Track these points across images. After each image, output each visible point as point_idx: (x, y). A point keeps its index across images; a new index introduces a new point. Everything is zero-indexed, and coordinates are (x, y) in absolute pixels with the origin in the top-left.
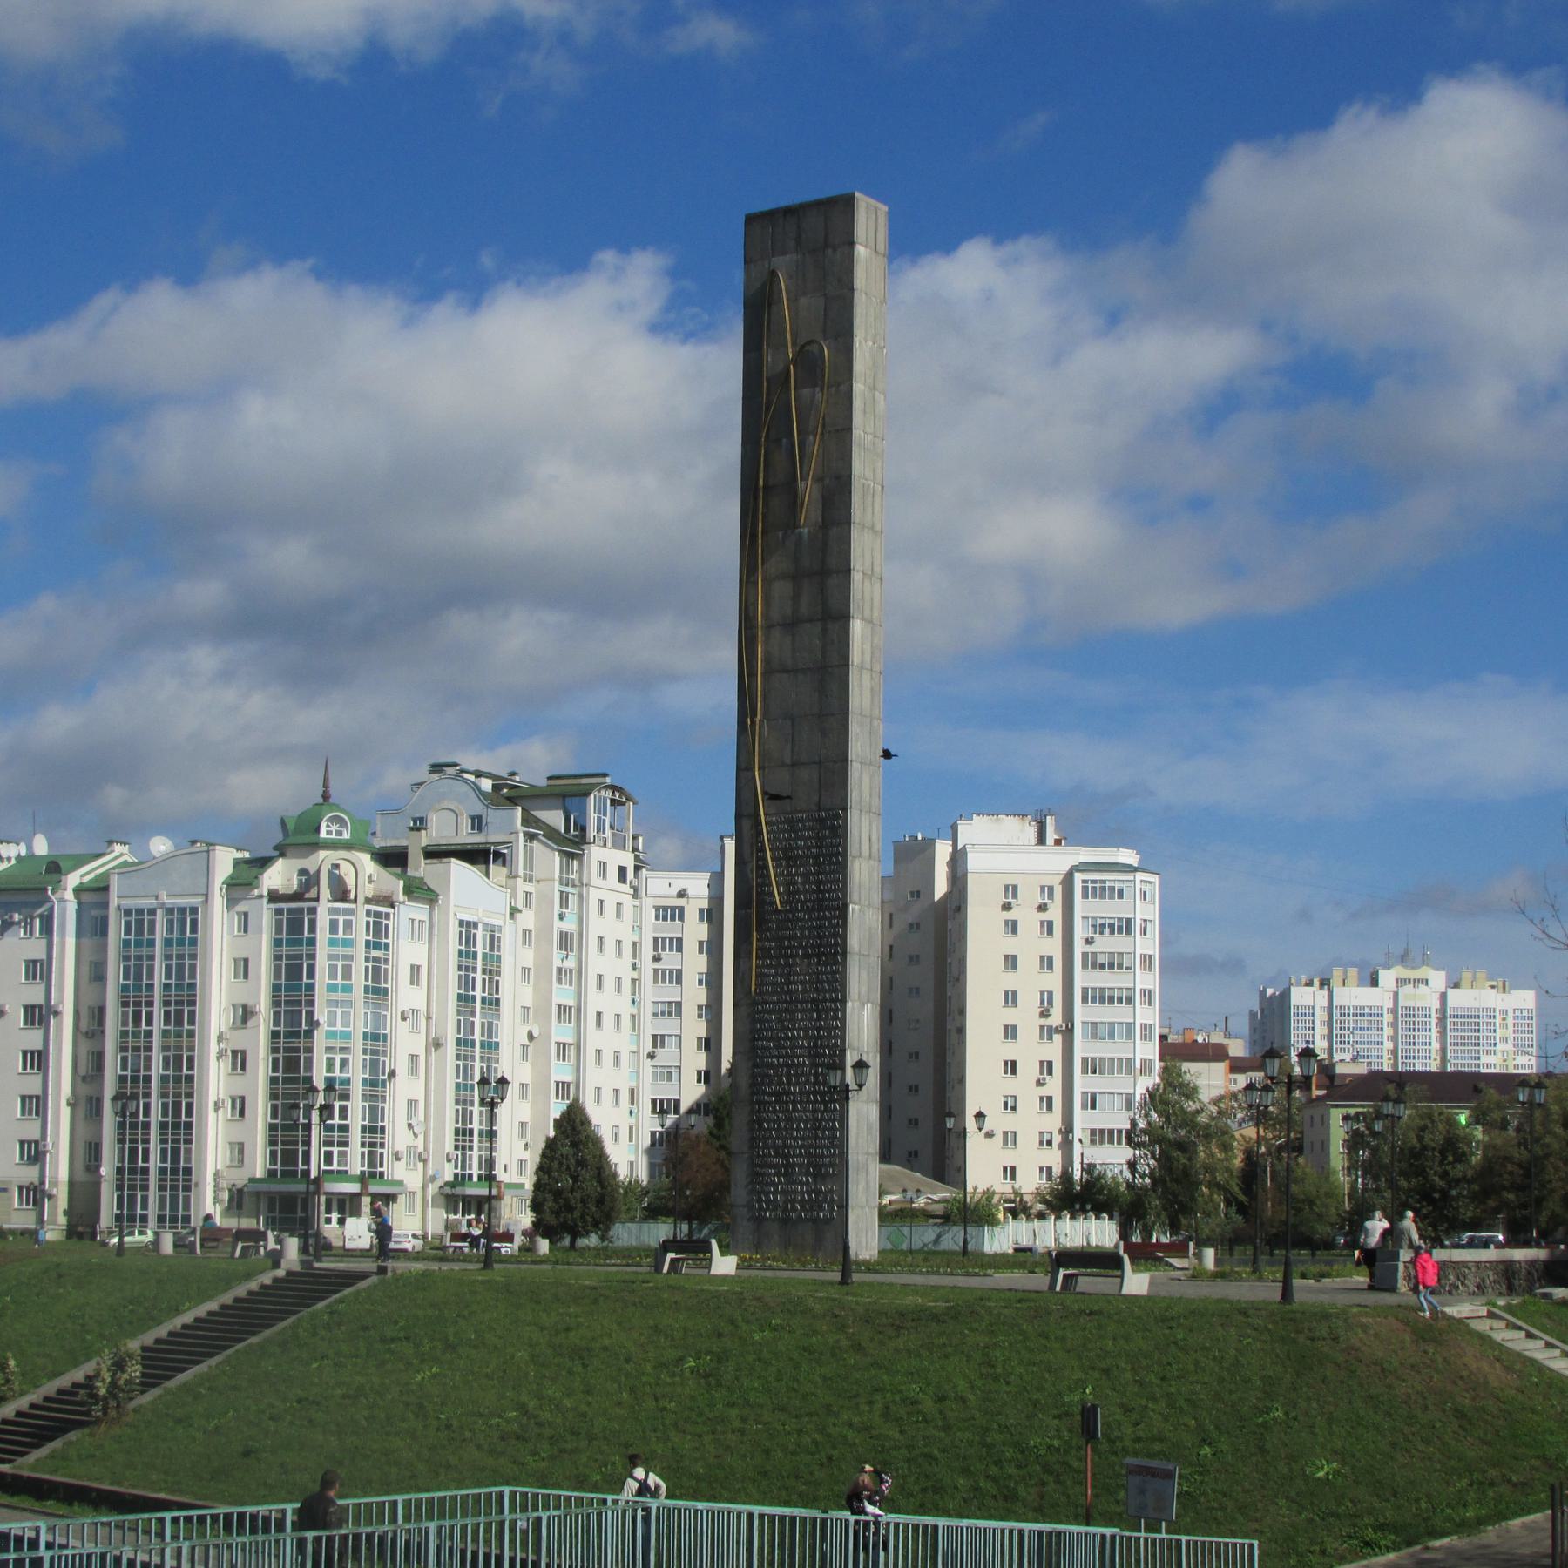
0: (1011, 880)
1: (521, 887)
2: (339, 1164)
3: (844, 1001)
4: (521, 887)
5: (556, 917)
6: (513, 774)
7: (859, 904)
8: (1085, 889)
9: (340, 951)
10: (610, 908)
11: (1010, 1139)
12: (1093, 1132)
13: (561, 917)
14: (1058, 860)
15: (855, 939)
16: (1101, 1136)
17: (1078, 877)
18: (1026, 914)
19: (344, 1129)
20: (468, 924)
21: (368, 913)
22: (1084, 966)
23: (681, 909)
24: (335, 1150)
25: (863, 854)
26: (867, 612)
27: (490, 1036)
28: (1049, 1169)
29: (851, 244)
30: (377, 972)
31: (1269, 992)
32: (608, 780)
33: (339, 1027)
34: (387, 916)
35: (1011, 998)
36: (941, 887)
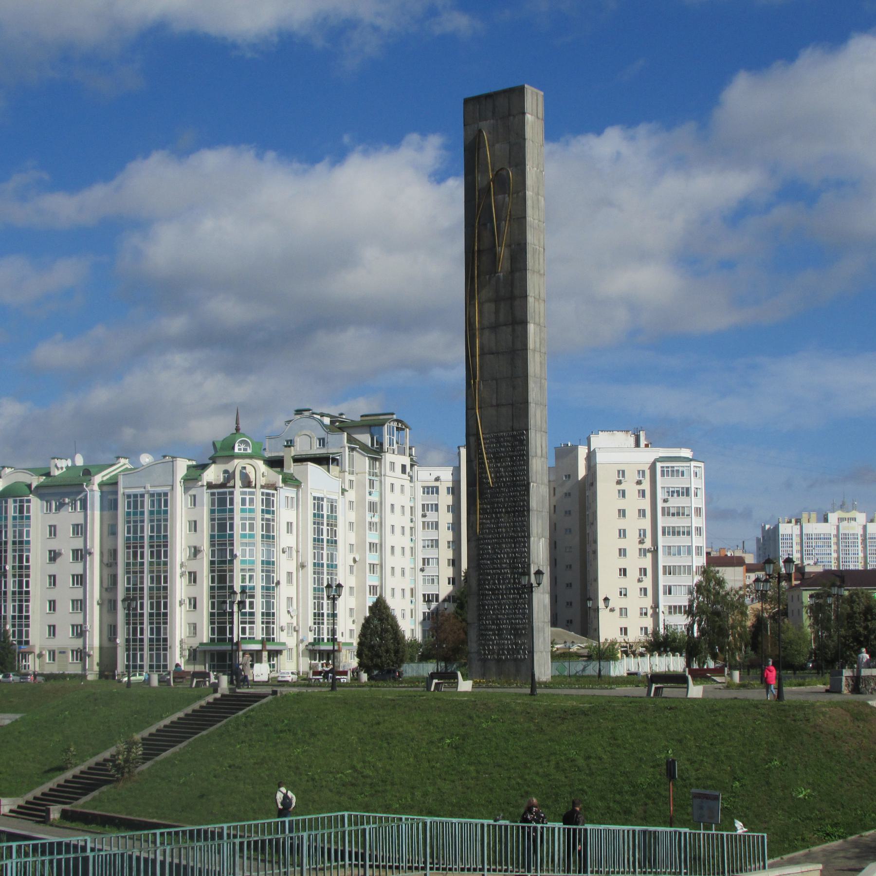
0: (621, 468)
3: (529, 537)
5: (367, 494)
6: (342, 414)
8: (663, 472)
10: (397, 488)
11: (624, 612)
12: (670, 607)
13: (370, 494)
14: (647, 456)
15: (534, 503)
16: (674, 609)
20: (318, 498)
21: (263, 494)
22: (663, 514)
23: (437, 488)
24: (247, 626)
26: (537, 320)
27: (332, 561)
28: (646, 628)
29: (524, 114)
30: (268, 527)
31: (767, 527)
32: (395, 417)
33: (248, 558)
34: (273, 495)
35: (622, 533)
36: (582, 473)
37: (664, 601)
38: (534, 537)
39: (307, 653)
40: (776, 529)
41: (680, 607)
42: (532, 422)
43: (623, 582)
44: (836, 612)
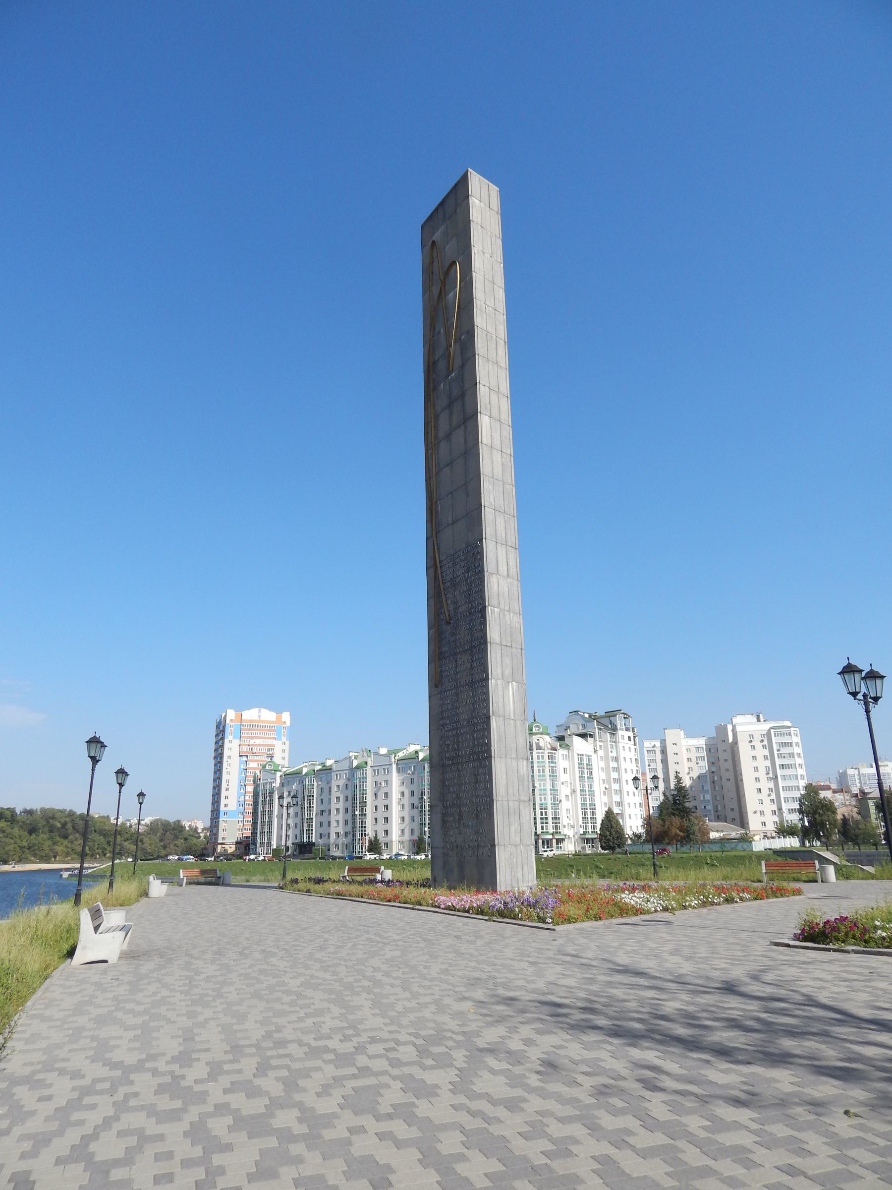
0: (751, 733)
1: (598, 743)
2: (546, 829)
3: (487, 679)
4: (598, 743)
5: (610, 752)
7: (499, 607)
8: (775, 734)
9: (541, 764)
10: (627, 749)
11: (762, 813)
12: (789, 810)
13: (611, 752)
14: (764, 727)
16: (791, 811)
17: (772, 731)
18: (757, 743)
19: (546, 818)
20: (581, 755)
21: (549, 753)
22: (778, 758)
23: (655, 750)
25: (501, 572)
27: (591, 788)
28: (776, 822)
30: (553, 771)
31: (841, 771)
32: (622, 712)
33: (542, 788)
34: (555, 754)
35: (756, 769)
36: (731, 740)
37: (785, 807)
38: (496, 679)
39: (580, 840)
40: (846, 771)
41: (795, 809)
42: (488, 530)
43: (760, 796)
44: (203, 1117)
